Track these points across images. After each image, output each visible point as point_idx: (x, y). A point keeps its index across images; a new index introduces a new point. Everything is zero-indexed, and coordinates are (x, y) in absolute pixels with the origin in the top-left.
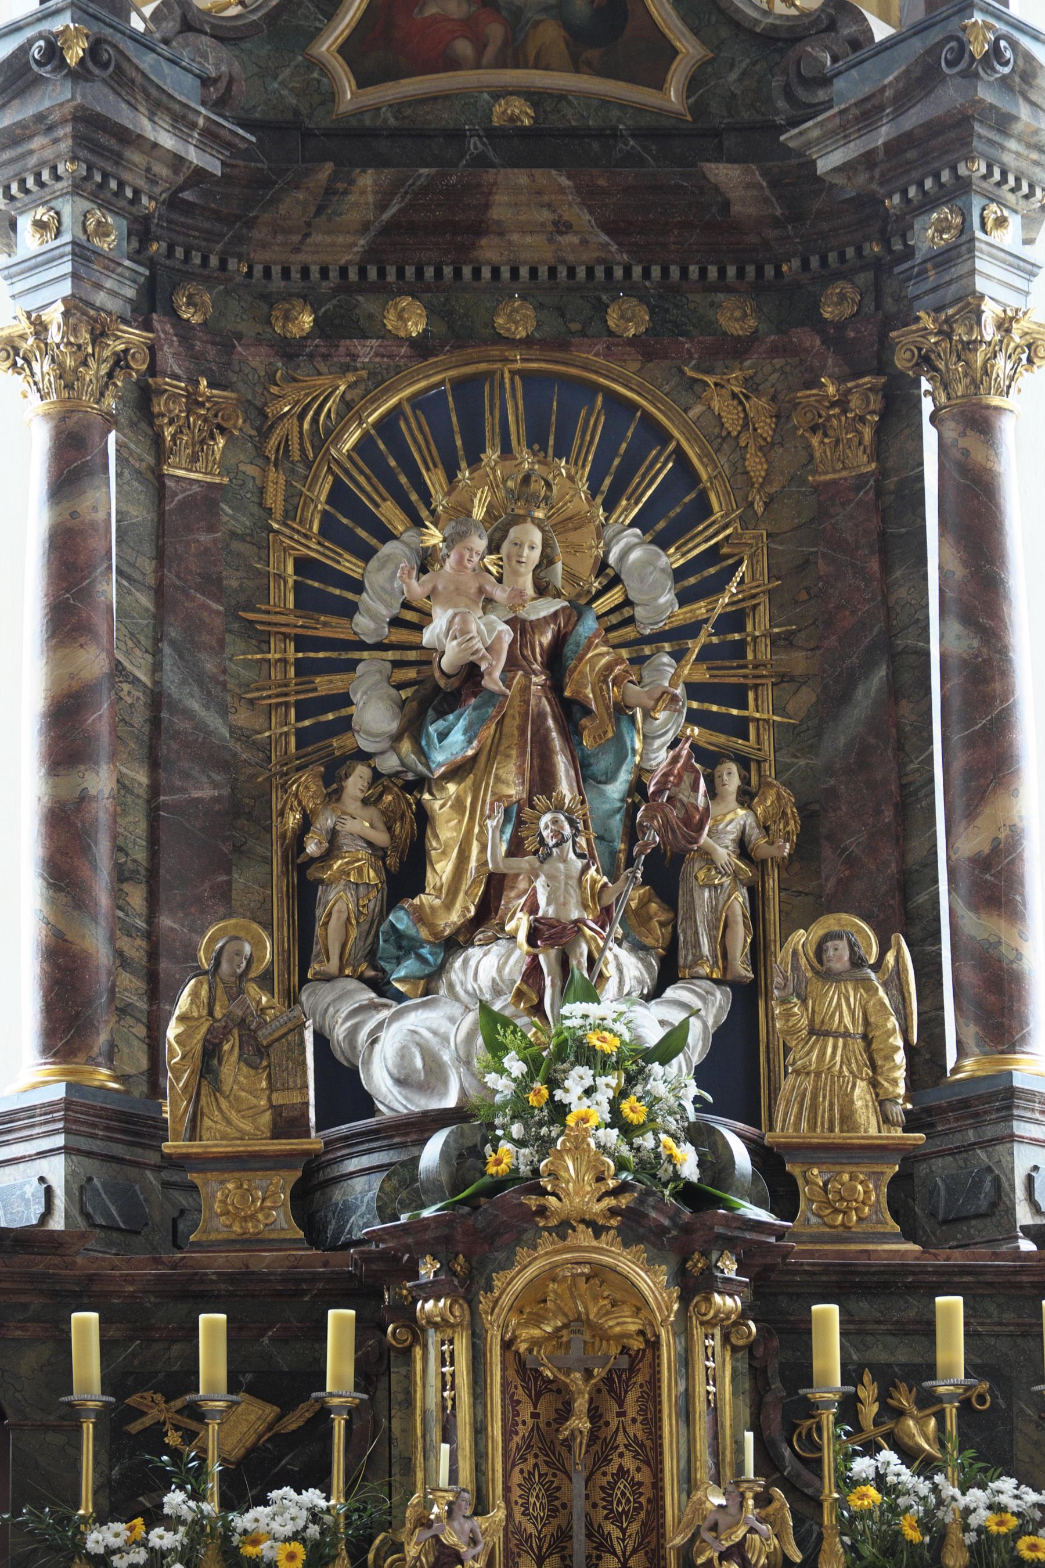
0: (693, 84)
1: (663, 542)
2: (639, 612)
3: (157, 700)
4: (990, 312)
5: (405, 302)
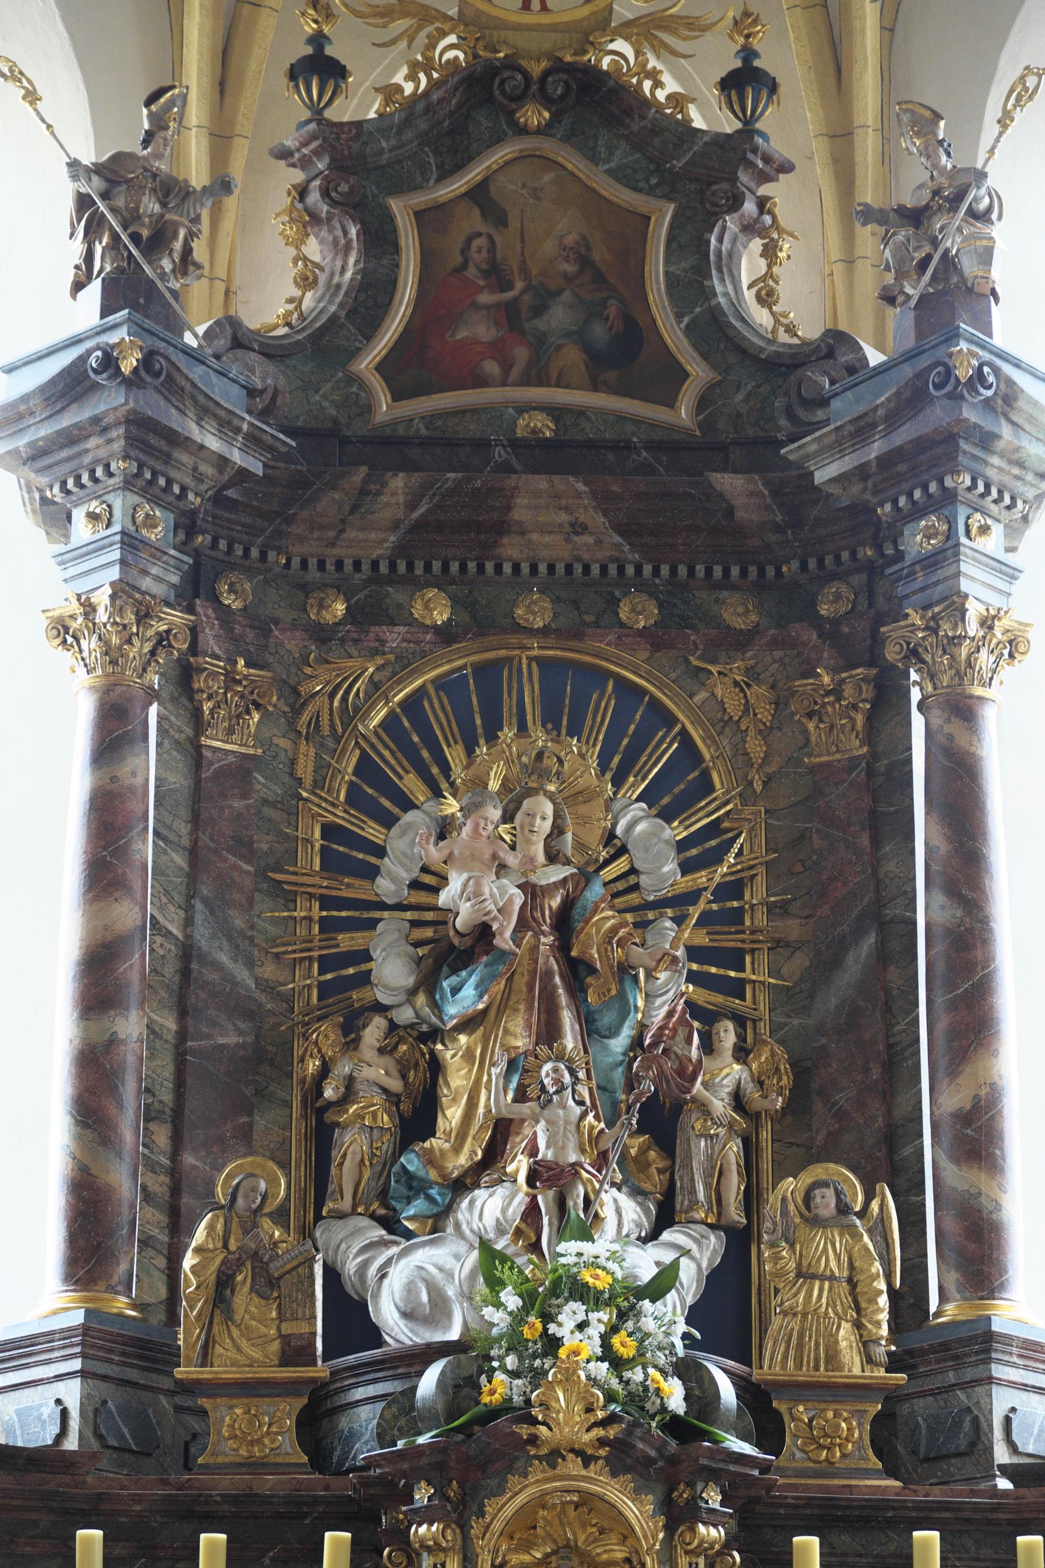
0: (702, 403)
1: (667, 815)
2: (644, 880)
4: (974, 610)
5: (431, 593)
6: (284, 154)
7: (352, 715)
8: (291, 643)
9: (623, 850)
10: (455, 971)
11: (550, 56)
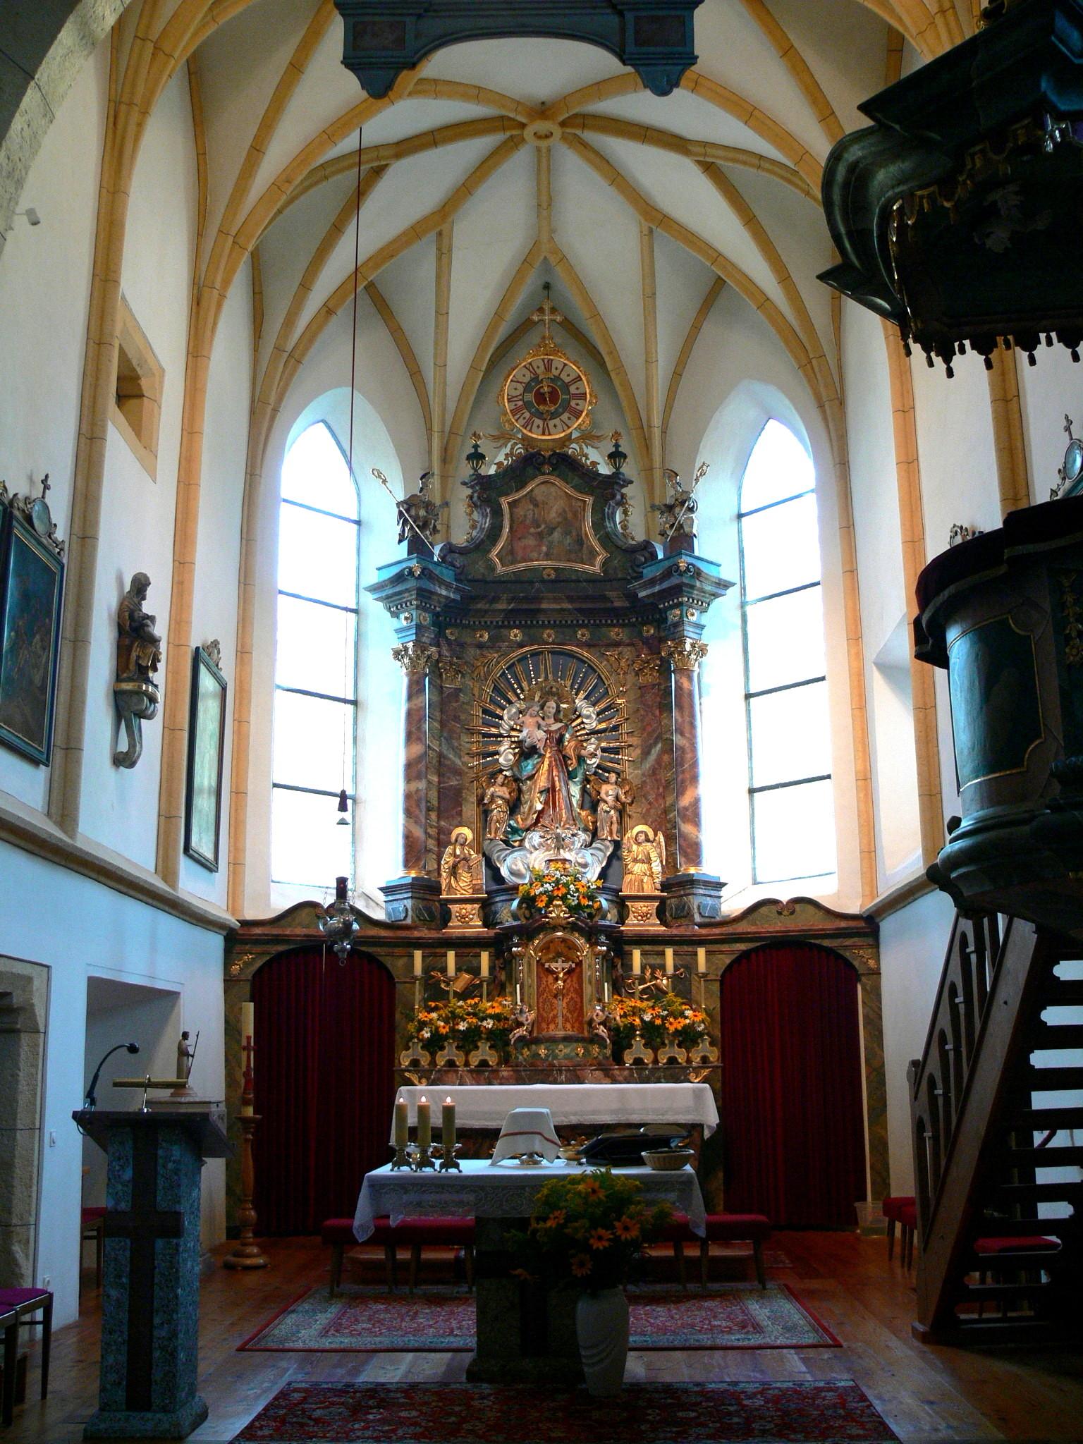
0: (604, 564)
1: (594, 705)
4: (688, 641)
6: (464, 483)
11: (552, 450)
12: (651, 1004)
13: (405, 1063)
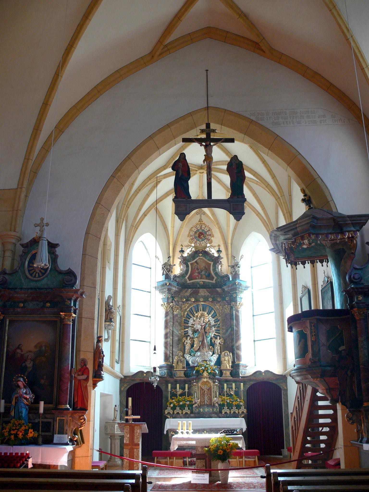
0: (215, 280)
1: (213, 318)
2: (211, 324)
3: (173, 331)
4: (238, 302)
5: (193, 298)
6: (178, 258)
7: (186, 310)
8: (181, 303)
9: (209, 321)
10: (195, 333)
12: (229, 398)
13: (166, 412)
